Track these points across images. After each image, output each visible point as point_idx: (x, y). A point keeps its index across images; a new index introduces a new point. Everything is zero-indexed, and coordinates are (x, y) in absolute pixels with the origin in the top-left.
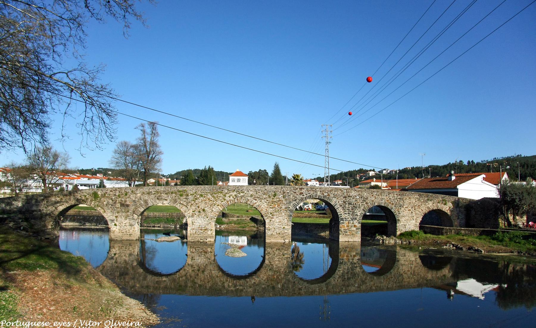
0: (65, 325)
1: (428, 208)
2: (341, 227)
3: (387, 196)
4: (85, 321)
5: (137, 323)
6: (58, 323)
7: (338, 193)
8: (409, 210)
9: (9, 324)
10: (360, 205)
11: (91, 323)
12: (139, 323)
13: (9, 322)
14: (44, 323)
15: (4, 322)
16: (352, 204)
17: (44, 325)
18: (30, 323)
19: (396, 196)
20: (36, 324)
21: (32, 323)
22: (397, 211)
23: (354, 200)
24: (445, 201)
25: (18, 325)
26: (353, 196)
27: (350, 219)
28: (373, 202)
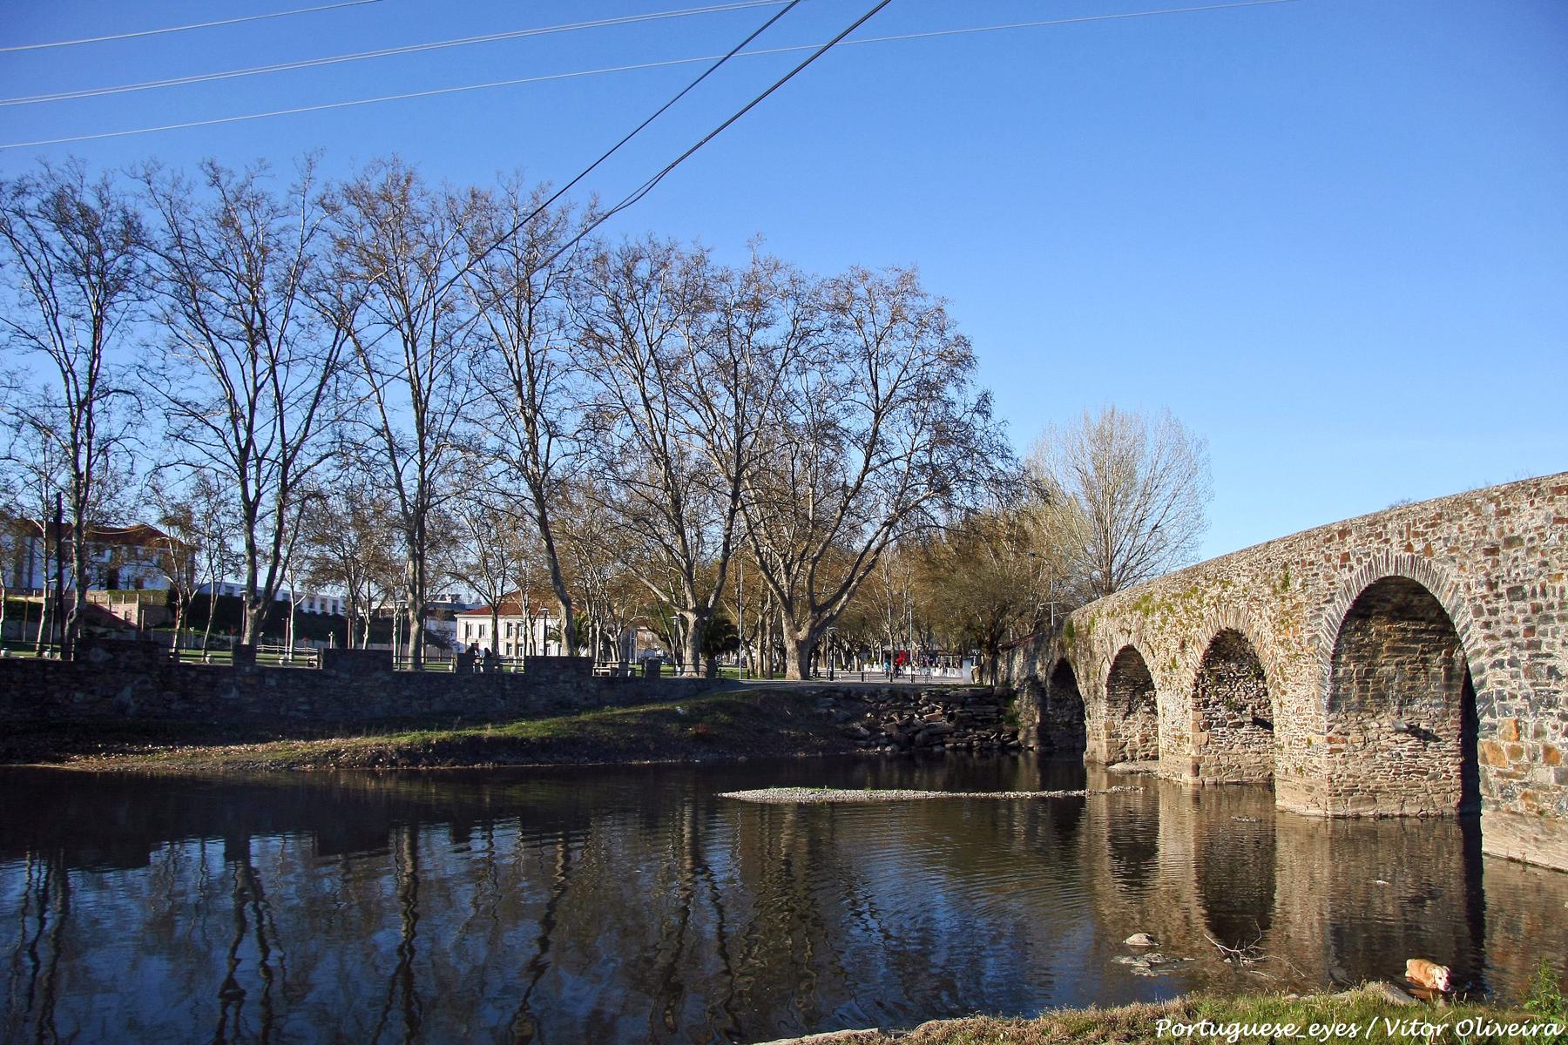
0: (1513, 1032)
2: (1485, 761)
4: (1398, 1021)
6: (1321, 1028)
7: (1461, 528)
13: (1180, 1025)
14: (1281, 1028)
16: (1524, 597)
17: (1280, 1032)
18: (1241, 1027)
20: (1258, 1030)
21: (1246, 1027)
23: (1533, 563)
25: (1205, 1031)
26: (1526, 537)
27: (1518, 703)
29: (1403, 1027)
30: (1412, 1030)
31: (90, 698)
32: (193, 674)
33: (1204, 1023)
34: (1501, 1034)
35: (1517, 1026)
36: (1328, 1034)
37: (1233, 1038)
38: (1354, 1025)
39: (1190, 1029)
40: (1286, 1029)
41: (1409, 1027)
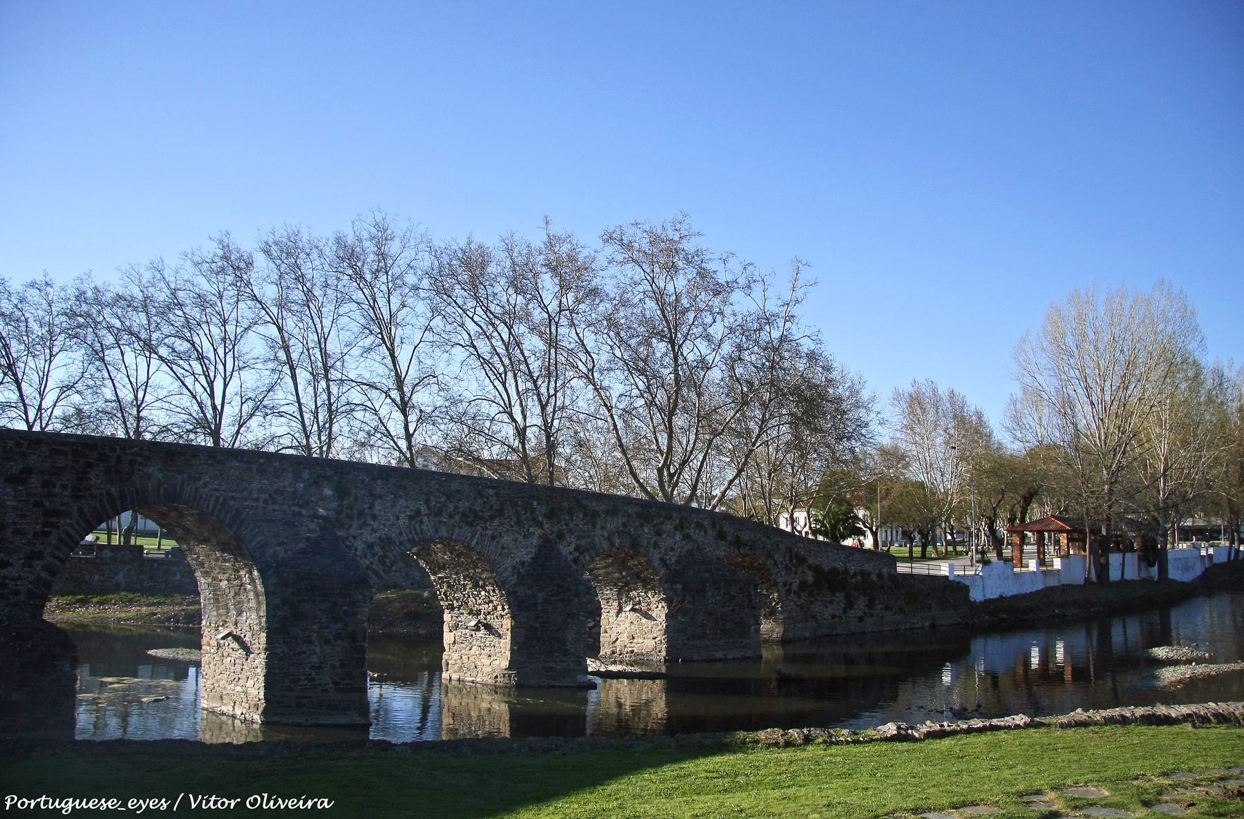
4: (200, 797)
18: (73, 802)
25: (44, 805)
29: (204, 801)
30: (211, 803)
31: (102, 578)
32: (156, 565)
33: (44, 798)
34: (282, 807)
35: (296, 801)
36: (144, 807)
37: (66, 811)
38: (164, 800)
39: (33, 803)
40: (109, 803)
41: (208, 802)
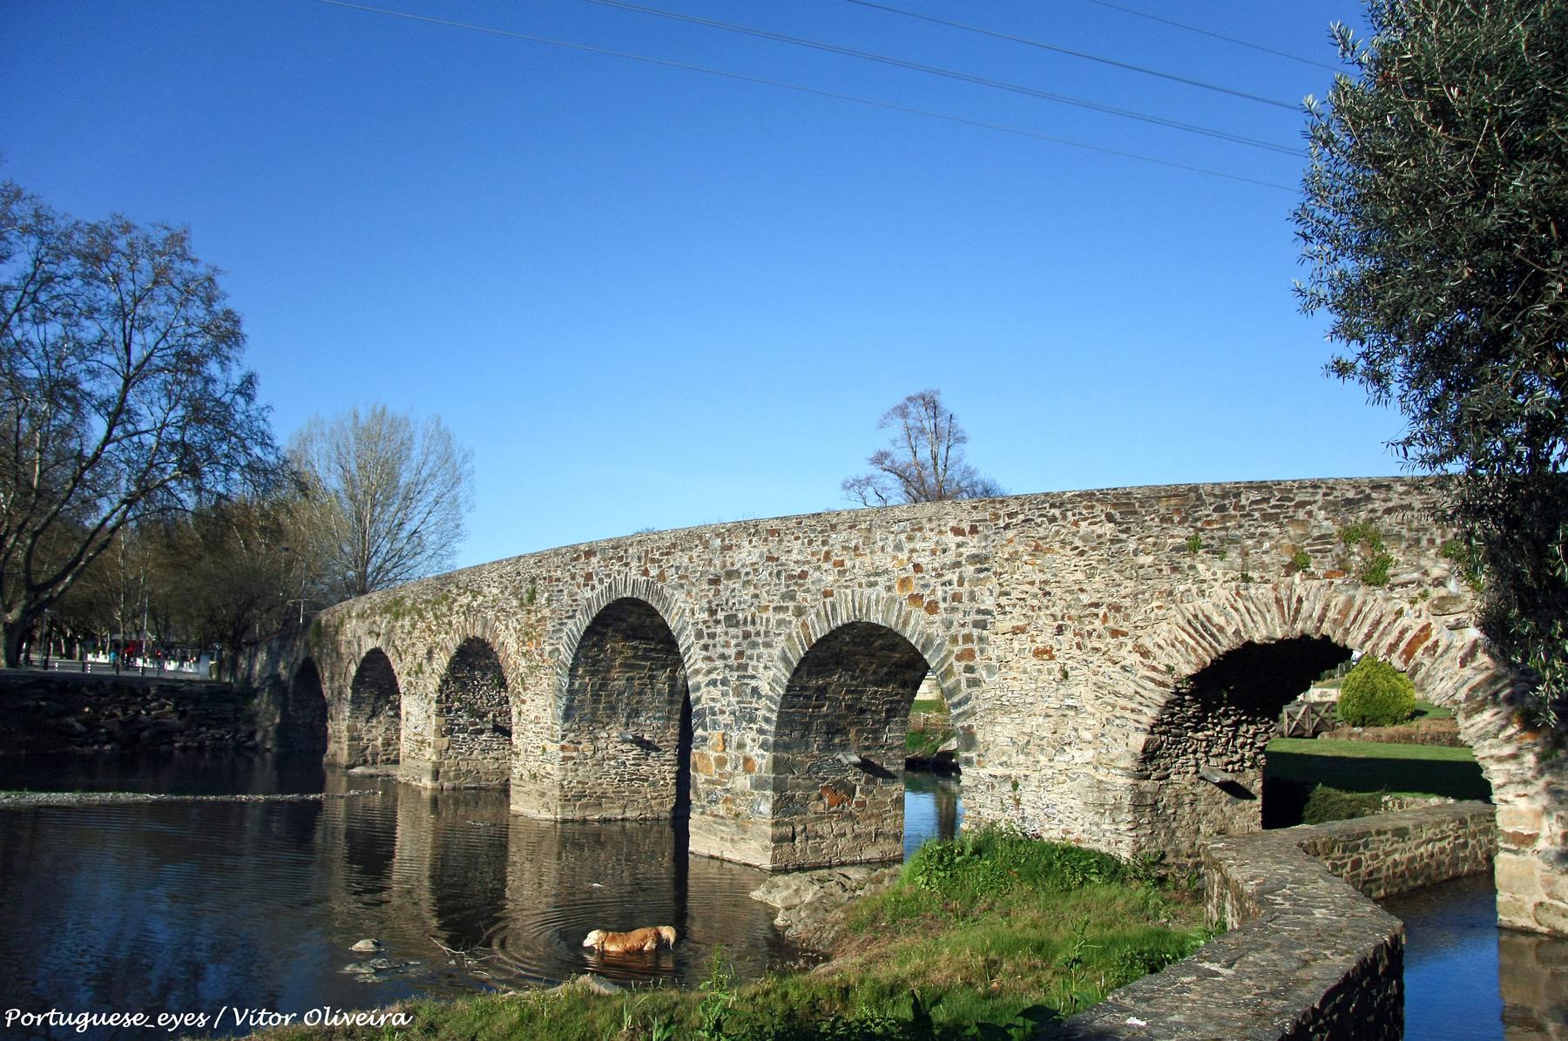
1: (1202, 627)
2: (696, 770)
3: (898, 547)
5: (398, 1017)
8: (1038, 653)
9: (27, 1020)
10: (773, 622)
11: (266, 1018)
12: (403, 1015)
15: (15, 1014)
18: (90, 1017)
19: (951, 540)
22: (959, 666)
24: (1373, 540)
26: (744, 571)
28: (828, 600)
